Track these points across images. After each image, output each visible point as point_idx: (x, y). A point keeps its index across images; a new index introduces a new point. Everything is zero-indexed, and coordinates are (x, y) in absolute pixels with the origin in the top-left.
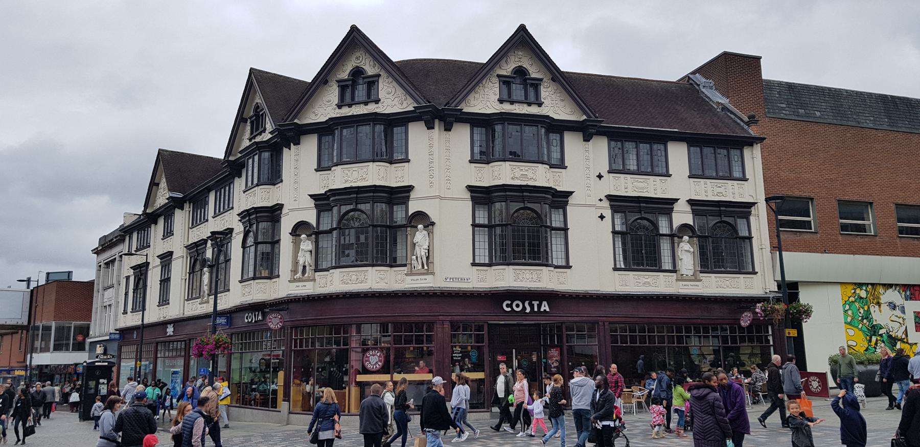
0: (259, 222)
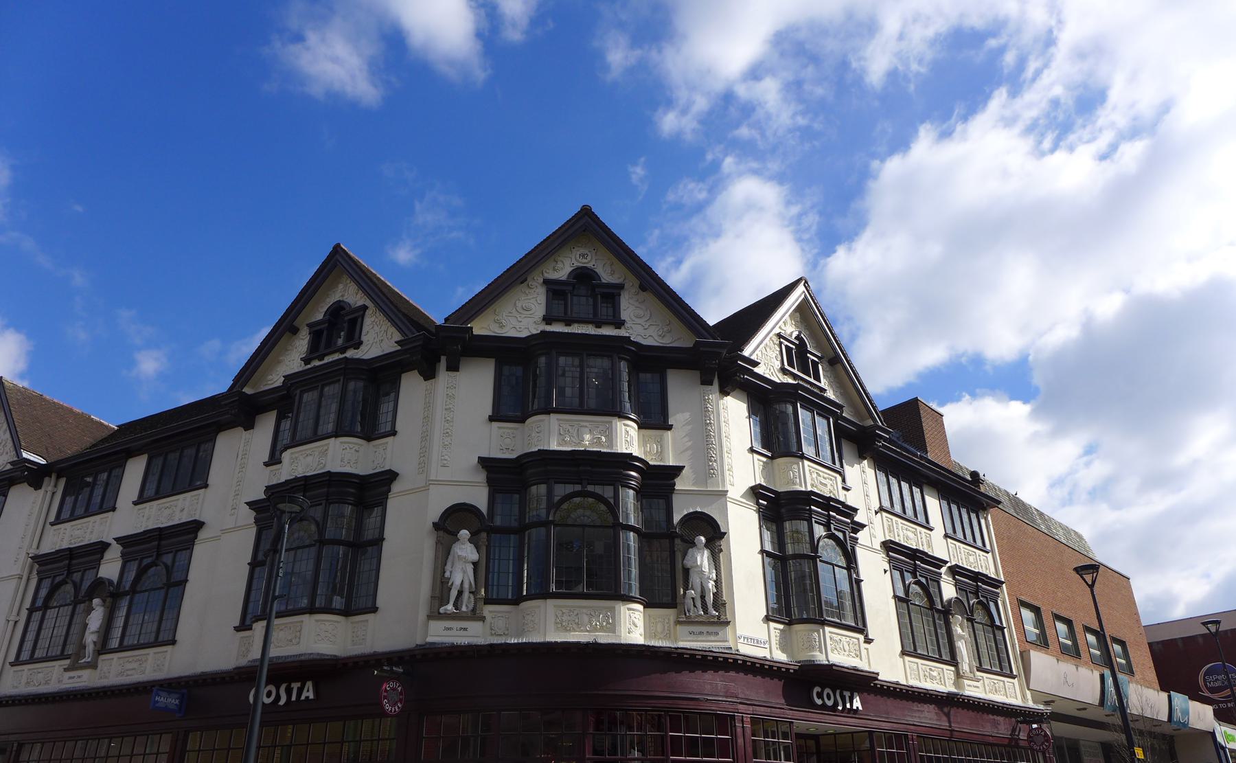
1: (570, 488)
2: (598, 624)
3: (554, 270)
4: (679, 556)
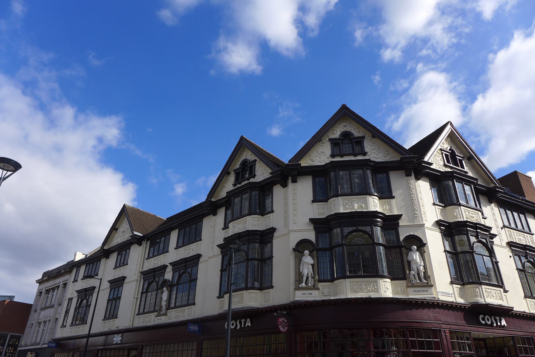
0: (250, 243)
1: (351, 229)
2: (370, 289)
3: (333, 134)
4: (405, 256)
